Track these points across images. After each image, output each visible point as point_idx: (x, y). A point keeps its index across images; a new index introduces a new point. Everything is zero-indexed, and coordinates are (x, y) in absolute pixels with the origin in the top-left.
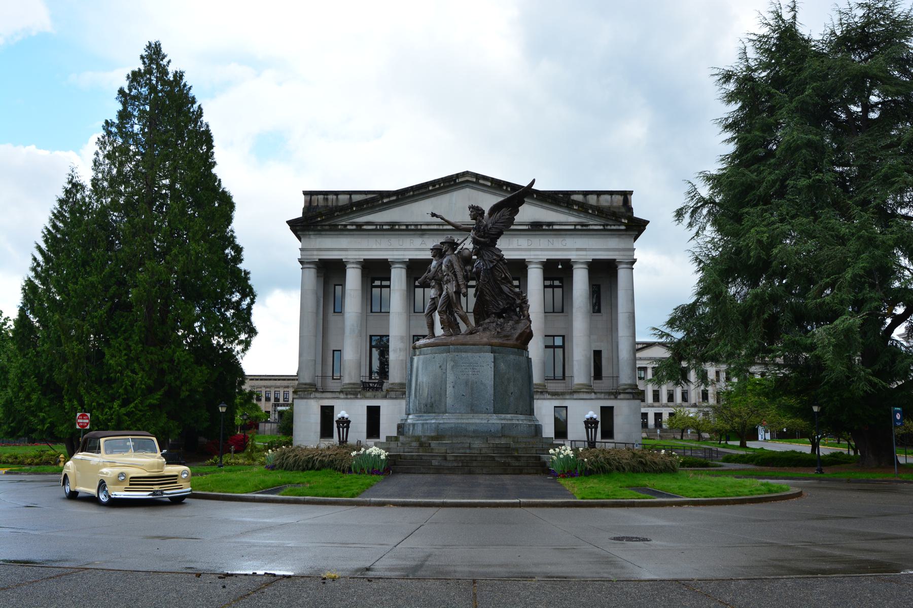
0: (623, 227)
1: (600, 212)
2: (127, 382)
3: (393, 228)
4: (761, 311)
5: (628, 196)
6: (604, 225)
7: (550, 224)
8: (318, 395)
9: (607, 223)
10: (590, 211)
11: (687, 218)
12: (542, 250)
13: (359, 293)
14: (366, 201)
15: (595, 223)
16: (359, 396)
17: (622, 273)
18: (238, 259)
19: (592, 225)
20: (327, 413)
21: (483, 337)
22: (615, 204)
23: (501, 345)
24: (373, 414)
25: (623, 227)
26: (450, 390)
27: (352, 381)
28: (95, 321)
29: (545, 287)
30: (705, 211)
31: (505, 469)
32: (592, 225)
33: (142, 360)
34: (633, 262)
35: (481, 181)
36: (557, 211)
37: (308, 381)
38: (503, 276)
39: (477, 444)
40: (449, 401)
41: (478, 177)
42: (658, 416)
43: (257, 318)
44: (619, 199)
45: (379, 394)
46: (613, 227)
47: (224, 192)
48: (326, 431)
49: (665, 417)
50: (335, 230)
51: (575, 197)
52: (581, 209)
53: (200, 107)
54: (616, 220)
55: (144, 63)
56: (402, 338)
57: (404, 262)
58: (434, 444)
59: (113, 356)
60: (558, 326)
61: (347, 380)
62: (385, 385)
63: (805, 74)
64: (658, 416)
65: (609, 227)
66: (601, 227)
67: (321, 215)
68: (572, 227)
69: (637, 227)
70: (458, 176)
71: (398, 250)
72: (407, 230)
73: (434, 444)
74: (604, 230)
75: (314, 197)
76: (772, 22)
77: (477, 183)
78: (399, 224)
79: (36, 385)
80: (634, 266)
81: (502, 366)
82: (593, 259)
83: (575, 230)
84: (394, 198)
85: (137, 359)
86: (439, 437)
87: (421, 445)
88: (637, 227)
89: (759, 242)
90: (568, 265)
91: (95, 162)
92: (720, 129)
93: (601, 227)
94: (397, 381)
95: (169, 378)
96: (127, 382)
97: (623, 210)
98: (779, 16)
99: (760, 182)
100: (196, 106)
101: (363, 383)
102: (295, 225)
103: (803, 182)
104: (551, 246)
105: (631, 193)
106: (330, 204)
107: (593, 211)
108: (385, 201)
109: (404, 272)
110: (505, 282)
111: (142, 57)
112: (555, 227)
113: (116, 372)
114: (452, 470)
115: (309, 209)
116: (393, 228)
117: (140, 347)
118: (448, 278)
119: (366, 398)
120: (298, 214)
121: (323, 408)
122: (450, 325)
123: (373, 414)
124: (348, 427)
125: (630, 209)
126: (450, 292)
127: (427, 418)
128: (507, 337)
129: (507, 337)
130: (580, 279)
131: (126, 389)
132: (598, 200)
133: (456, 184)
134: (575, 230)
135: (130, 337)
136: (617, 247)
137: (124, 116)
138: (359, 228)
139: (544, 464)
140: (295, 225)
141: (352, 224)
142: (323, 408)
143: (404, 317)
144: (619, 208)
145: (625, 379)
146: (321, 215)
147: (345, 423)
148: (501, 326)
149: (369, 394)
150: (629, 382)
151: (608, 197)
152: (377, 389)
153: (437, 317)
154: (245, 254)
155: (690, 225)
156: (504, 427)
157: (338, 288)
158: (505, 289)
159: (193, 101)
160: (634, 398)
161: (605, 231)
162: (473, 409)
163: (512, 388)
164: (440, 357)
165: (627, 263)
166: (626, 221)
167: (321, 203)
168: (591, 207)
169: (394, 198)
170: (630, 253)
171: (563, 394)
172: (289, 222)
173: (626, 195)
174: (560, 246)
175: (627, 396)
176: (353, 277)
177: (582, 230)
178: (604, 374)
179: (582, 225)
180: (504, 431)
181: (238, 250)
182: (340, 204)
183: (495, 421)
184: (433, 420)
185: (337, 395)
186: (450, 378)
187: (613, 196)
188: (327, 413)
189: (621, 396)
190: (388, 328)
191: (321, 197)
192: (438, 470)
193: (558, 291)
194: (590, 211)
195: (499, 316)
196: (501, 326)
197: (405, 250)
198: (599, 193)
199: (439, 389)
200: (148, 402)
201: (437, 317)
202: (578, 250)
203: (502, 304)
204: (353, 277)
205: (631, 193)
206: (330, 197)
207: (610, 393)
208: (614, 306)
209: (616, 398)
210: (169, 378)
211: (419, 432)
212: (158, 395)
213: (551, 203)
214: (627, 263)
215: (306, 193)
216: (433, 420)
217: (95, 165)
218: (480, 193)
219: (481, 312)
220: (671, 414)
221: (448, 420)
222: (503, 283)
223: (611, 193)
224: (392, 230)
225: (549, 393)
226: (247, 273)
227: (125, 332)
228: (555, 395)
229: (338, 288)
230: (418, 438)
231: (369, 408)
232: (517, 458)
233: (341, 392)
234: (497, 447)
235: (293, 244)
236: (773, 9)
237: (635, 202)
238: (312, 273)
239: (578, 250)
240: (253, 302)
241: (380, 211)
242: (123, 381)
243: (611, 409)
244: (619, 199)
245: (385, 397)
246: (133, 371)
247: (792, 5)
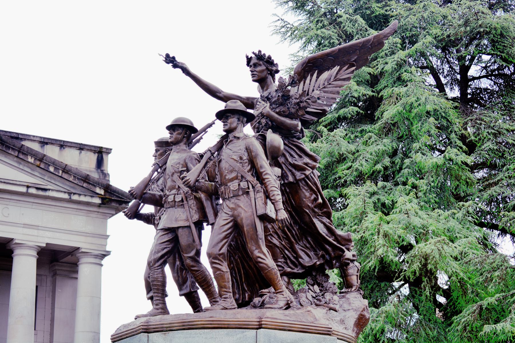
5: (104, 156)
6: (70, 194)
9: (74, 191)
10: (52, 169)
19: (52, 190)
25: (98, 201)
32: (52, 190)
38: (320, 200)
46: (83, 199)
52: (38, 163)
65: (75, 197)
66: (66, 196)
68: (23, 190)
74: (70, 201)
80: (103, 262)
82: (47, 244)
93: (66, 196)
105: (108, 151)
107: (56, 169)
110: (320, 212)
118: (244, 184)
125: (105, 175)
126: (243, 215)
136: (83, 230)
151: (75, 152)
165: (96, 256)
166: (102, 192)
168: (54, 163)
170: (101, 241)
187: (83, 152)
194: (52, 169)
198: (63, 145)
202: (26, 226)
205: (108, 151)
214: (96, 256)
222: (316, 215)
223: (81, 147)
239: (26, 226)
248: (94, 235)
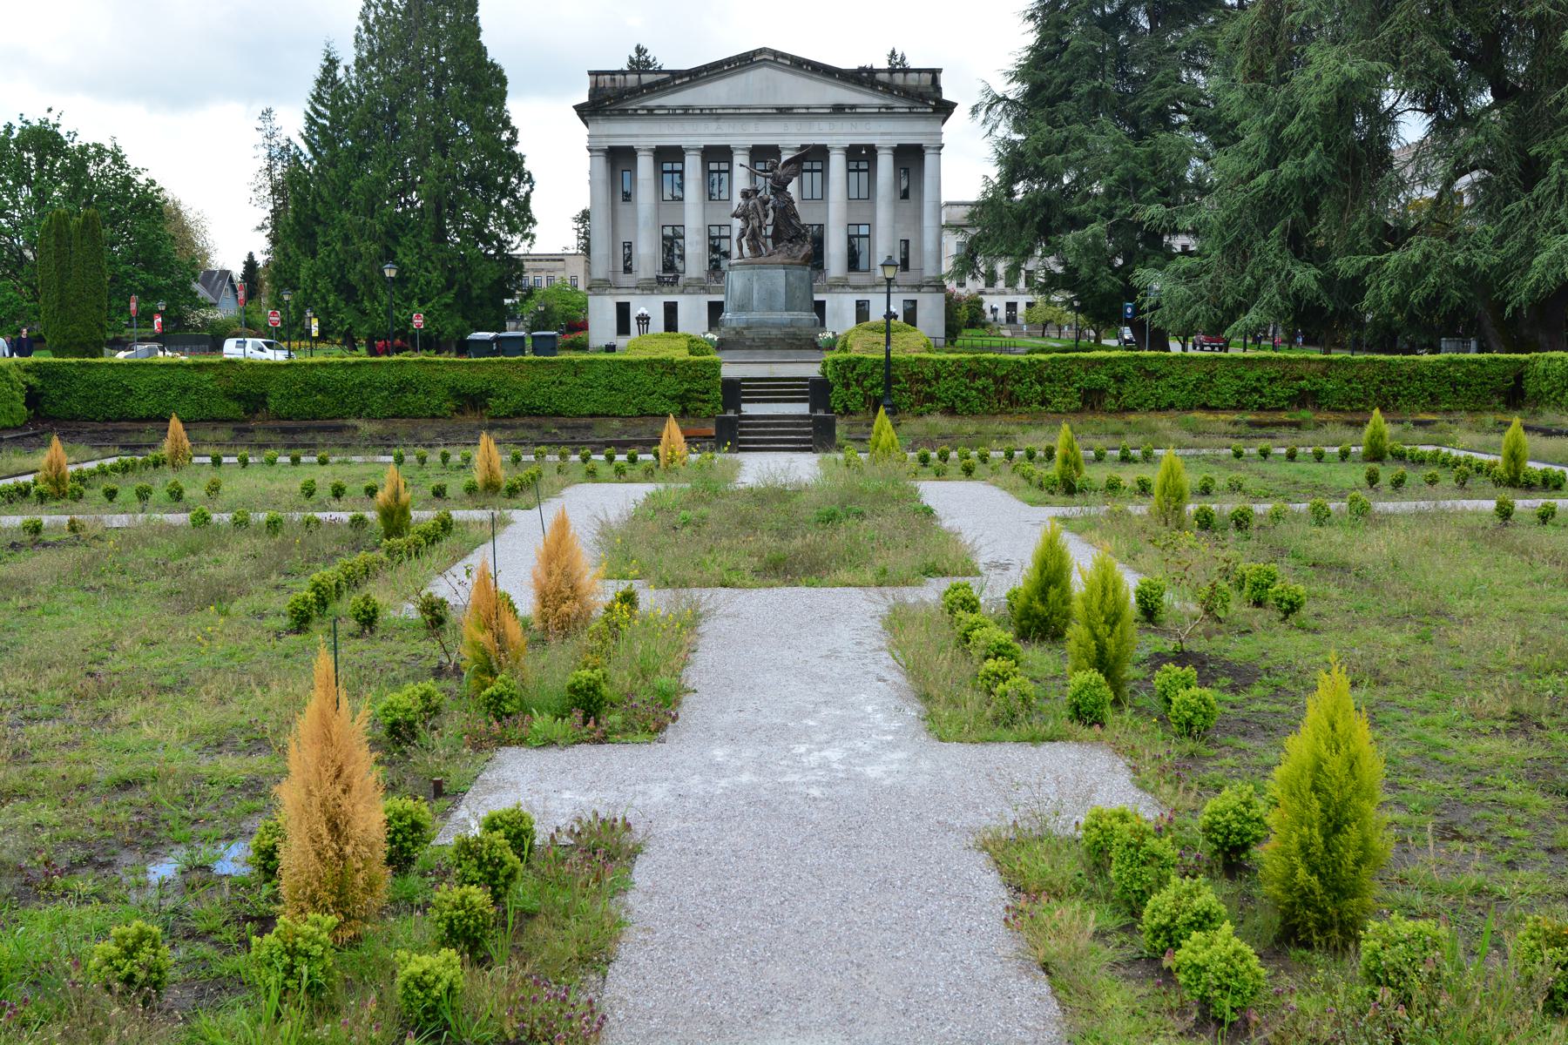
0: (930, 110)
1: (907, 93)
3: (686, 112)
4: (1034, 214)
7: (853, 107)
8: (613, 291)
11: (982, 115)
12: (845, 134)
13: (652, 182)
15: (901, 105)
16: (92, 150)
17: (929, 159)
18: (513, 141)
20: (623, 310)
21: (778, 258)
22: (923, 83)
24: (671, 310)
25: (930, 110)
28: (385, 218)
29: (849, 171)
31: (791, 346)
33: (433, 258)
34: (941, 147)
35: (780, 60)
36: (860, 92)
40: (755, 303)
41: (777, 54)
44: (928, 77)
45: (675, 288)
48: (623, 328)
49: (1021, 308)
51: (880, 76)
54: (923, 102)
56: (698, 230)
58: (745, 332)
59: (405, 255)
60: (861, 215)
64: (1011, 306)
67: (609, 98)
70: (755, 53)
71: (692, 135)
72: (701, 114)
73: (745, 332)
79: (330, 286)
81: (791, 278)
83: (879, 113)
85: (429, 258)
86: (748, 328)
87: (737, 333)
90: (872, 151)
91: (357, 38)
95: (460, 276)
96: (422, 280)
97: (931, 90)
99: (1050, 82)
101: (658, 277)
102: (581, 110)
103: (1085, 88)
104: (854, 131)
105: (940, 71)
106: (617, 85)
108: (677, 82)
109: (698, 160)
112: (858, 110)
113: (411, 272)
114: (758, 348)
115: (595, 91)
116: (686, 112)
119: (662, 293)
120: (584, 98)
121: (619, 305)
122: (755, 249)
123: (671, 310)
125: (939, 89)
127: (1452, 407)
128: (795, 258)
129: (795, 258)
131: (421, 288)
133: (752, 62)
134: (879, 113)
138: (650, 112)
139: (816, 344)
140: (581, 110)
141: (643, 108)
142: (619, 305)
144: (927, 87)
145: (929, 272)
146: (609, 98)
149: (666, 289)
150: (933, 274)
151: (915, 75)
153: (744, 241)
154: (520, 137)
155: (984, 122)
156: (792, 320)
157: (627, 174)
158: (794, 222)
161: (911, 114)
162: (771, 309)
164: (749, 272)
167: (608, 84)
168: (897, 87)
169: (687, 79)
171: (865, 287)
172: (575, 107)
173: (935, 73)
174: (864, 131)
175: (931, 289)
176: (645, 165)
177: (887, 112)
179: (887, 108)
180: (792, 323)
181: (514, 132)
184: (744, 316)
186: (756, 287)
188: (623, 310)
189: (925, 289)
190: (683, 216)
191: (607, 77)
192: (750, 347)
193: (864, 175)
195: (790, 241)
197: (699, 135)
199: (748, 292)
200: (443, 301)
201: (744, 241)
202: (882, 134)
203: (792, 233)
205: (940, 71)
206: (617, 77)
208: (920, 192)
211: (734, 324)
212: (451, 294)
215: (591, 73)
216: (744, 316)
217: (357, 41)
219: (777, 238)
220: (1029, 305)
221: (755, 316)
223: (919, 71)
227: (412, 229)
228: (857, 288)
229: (627, 174)
230: (734, 329)
233: (637, 288)
234: (787, 334)
235: (579, 132)
238: (601, 161)
239: (882, 134)
241: (673, 93)
242: (418, 280)
243: (914, 302)
245: (682, 292)
248: (932, 134)
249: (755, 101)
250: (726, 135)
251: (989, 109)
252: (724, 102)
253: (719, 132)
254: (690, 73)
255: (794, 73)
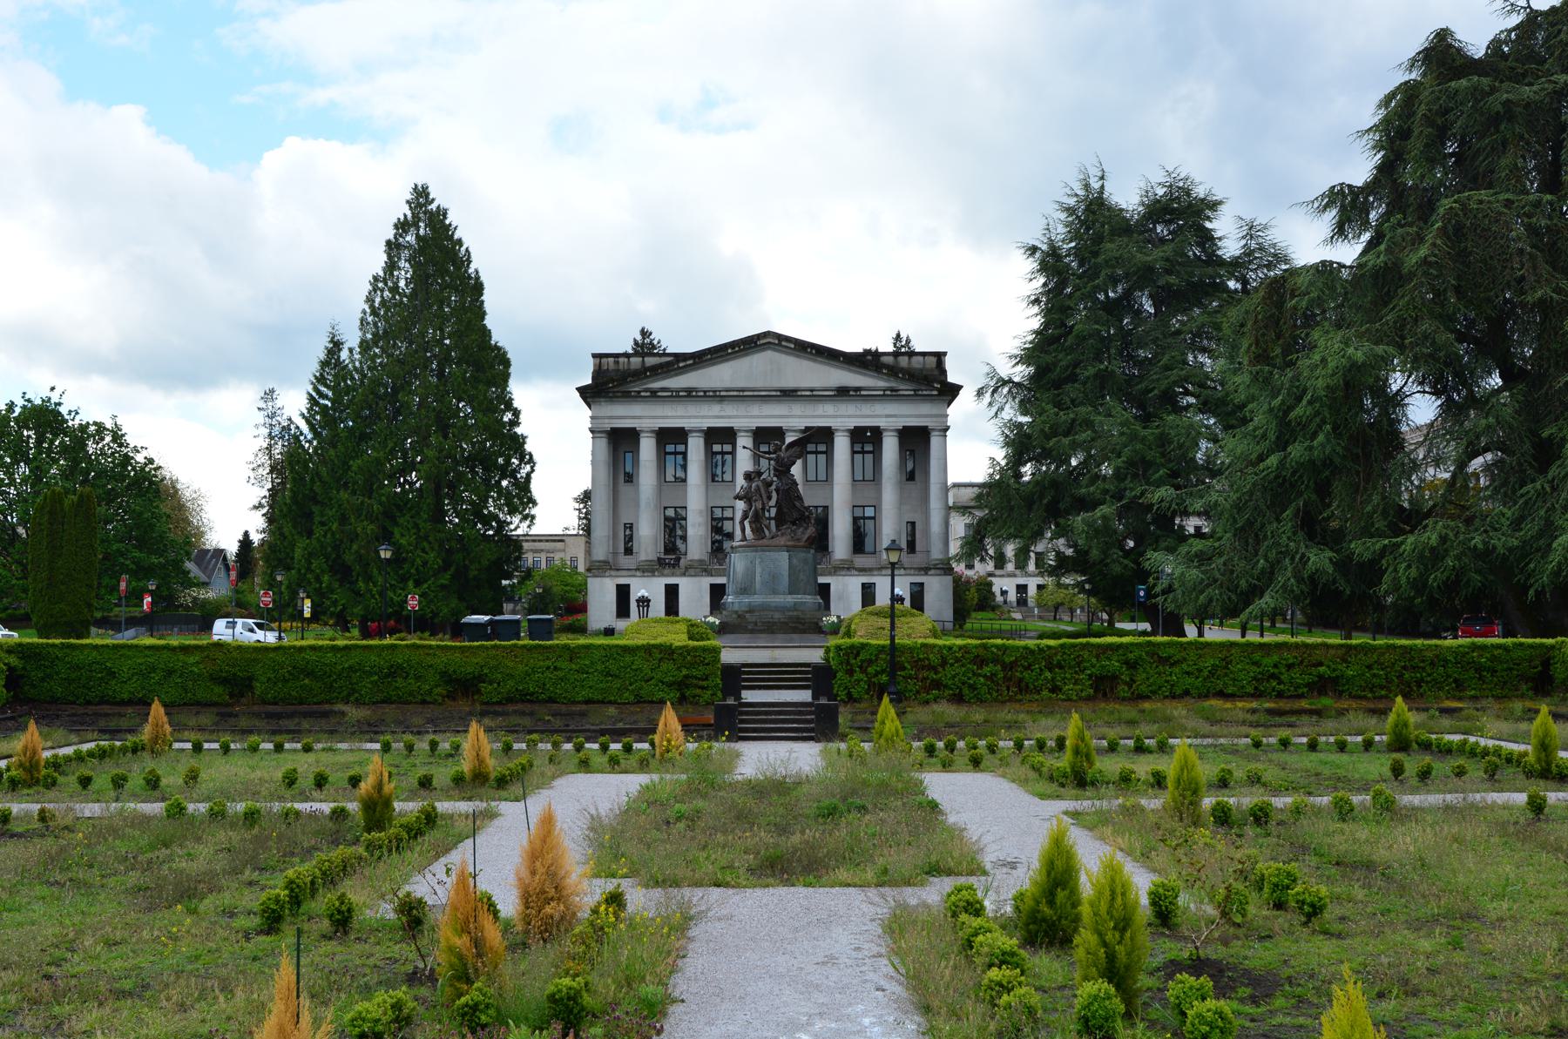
1: (911, 376)
2: (419, 561)
3: (690, 395)
4: (1042, 496)
8: (613, 573)
11: (988, 395)
12: (849, 416)
14: (661, 366)
15: (905, 388)
17: (935, 441)
18: (515, 422)
20: (623, 592)
21: (782, 541)
23: (795, 546)
26: (758, 578)
27: (650, 558)
28: (384, 499)
29: (854, 452)
30: (1006, 390)
31: (795, 630)
34: (947, 428)
36: (865, 375)
37: (602, 558)
39: (777, 616)
40: (758, 586)
42: (1022, 589)
43: (536, 488)
44: (932, 361)
45: (677, 571)
47: (499, 349)
48: (623, 610)
49: (1032, 591)
50: (628, 396)
51: (885, 359)
53: (467, 250)
55: (411, 208)
57: (701, 431)
58: (747, 616)
59: (402, 535)
61: (643, 557)
62: (682, 561)
63: (1100, 259)
64: (1022, 589)
69: (952, 391)
72: (705, 396)
73: (747, 616)
75: (604, 360)
76: (1079, 192)
77: (779, 344)
78: (696, 390)
79: (325, 566)
84: (691, 362)
85: (426, 538)
87: (739, 616)
88: (952, 391)
89: (1042, 430)
90: (877, 433)
91: (362, 320)
92: (1025, 304)
94: (696, 557)
96: (419, 561)
97: (936, 373)
98: (1087, 186)
100: (463, 249)
101: (659, 559)
103: (1091, 371)
104: (858, 413)
105: (945, 354)
106: (621, 367)
109: (702, 441)
111: (408, 202)
114: (761, 632)
115: (598, 374)
116: (690, 395)
117: (428, 526)
119: (663, 575)
120: (587, 380)
122: (758, 531)
123: (672, 592)
124: (648, 606)
125: (944, 372)
130: (890, 446)
131: (417, 569)
132: (910, 362)
133: (756, 345)
135: (419, 514)
137: (391, 266)
138: (654, 394)
143: (703, 489)
144: (932, 370)
145: (936, 554)
147: (644, 602)
148: (794, 532)
150: (940, 557)
151: (921, 358)
152: (674, 566)
153: (746, 523)
154: (522, 418)
155: (990, 404)
156: (795, 604)
157: (629, 456)
158: (797, 504)
159: (460, 242)
160: (945, 574)
161: (916, 397)
162: (775, 592)
163: (802, 576)
167: (612, 366)
168: (902, 370)
169: (691, 362)
174: (868, 413)
175: (938, 572)
176: (647, 447)
177: (891, 395)
178: (918, 548)
180: (795, 607)
181: (516, 413)
182: (632, 367)
183: (790, 599)
185: (633, 573)
186: (758, 570)
188: (623, 592)
189: (932, 572)
191: (611, 360)
192: (752, 632)
193: (869, 457)
195: (794, 523)
196: (794, 532)
197: (703, 417)
201: (746, 523)
202: (888, 416)
203: (795, 515)
204: (647, 447)
205: (945, 354)
206: (621, 360)
207: (920, 569)
208: (926, 473)
209: (926, 574)
210: (458, 557)
211: (736, 607)
213: (859, 367)
215: (595, 356)
217: (362, 324)
218: (783, 356)
219: (780, 520)
220: (1040, 587)
221: (757, 599)
224: (689, 396)
225: (856, 569)
226: (524, 438)
227: (410, 509)
228: (863, 571)
230: (736, 612)
231: (667, 586)
232: (803, 624)
233: (637, 570)
234: (791, 617)
236: (1082, 177)
237: (949, 364)
238: (603, 443)
239: (888, 416)
240: (533, 471)
241: (676, 375)
244: (932, 361)
245: (684, 575)
246: (423, 550)
247: (1100, 174)
249: (759, 384)
250: (729, 417)
251: (994, 391)
252: (728, 385)
253: (722, 414)
254: (693, 356)
255: (798, 356)
